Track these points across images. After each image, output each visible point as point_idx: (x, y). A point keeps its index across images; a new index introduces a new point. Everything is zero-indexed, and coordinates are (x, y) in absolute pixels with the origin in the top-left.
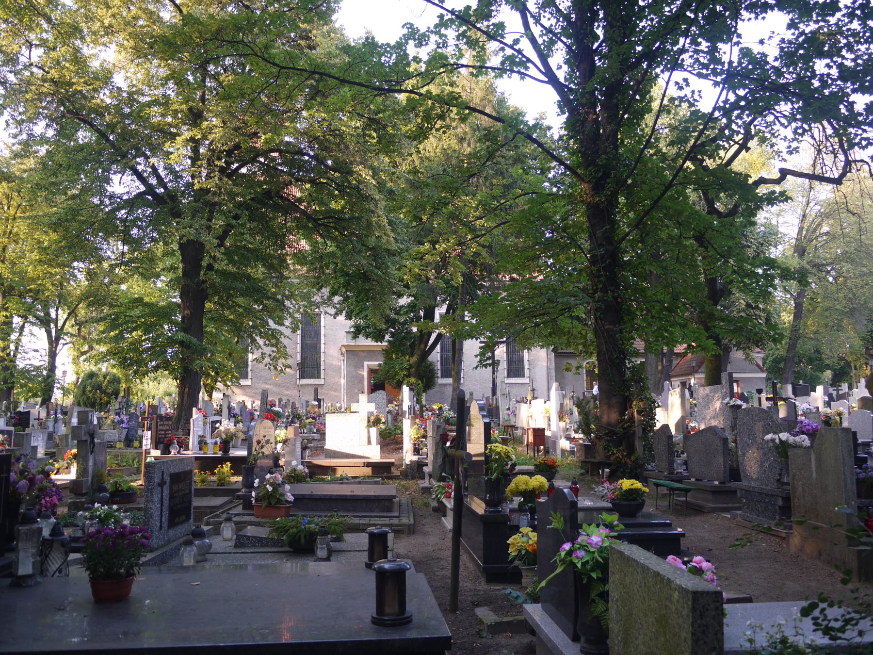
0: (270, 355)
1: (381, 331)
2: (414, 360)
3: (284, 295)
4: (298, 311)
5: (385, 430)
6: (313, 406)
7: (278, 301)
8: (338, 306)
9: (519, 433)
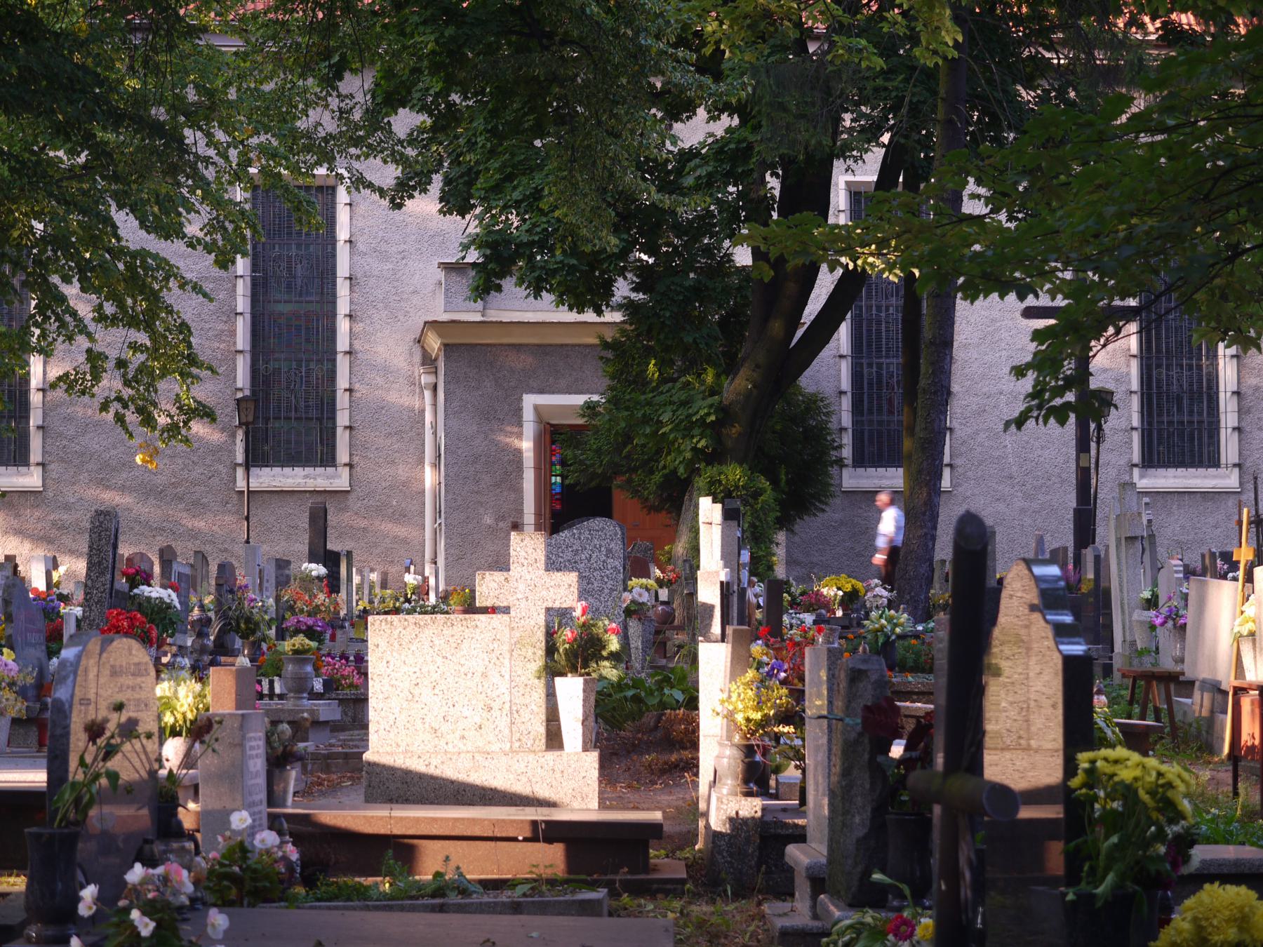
0: (121, 364)
1: (596, 259)
2: (738, 385)
3: (180, 105)
4: (239, 175)
5: (620, 686)
6: (308, 580)
7: (156, 128)
8: (411, 152)
9: (1197, 704)
